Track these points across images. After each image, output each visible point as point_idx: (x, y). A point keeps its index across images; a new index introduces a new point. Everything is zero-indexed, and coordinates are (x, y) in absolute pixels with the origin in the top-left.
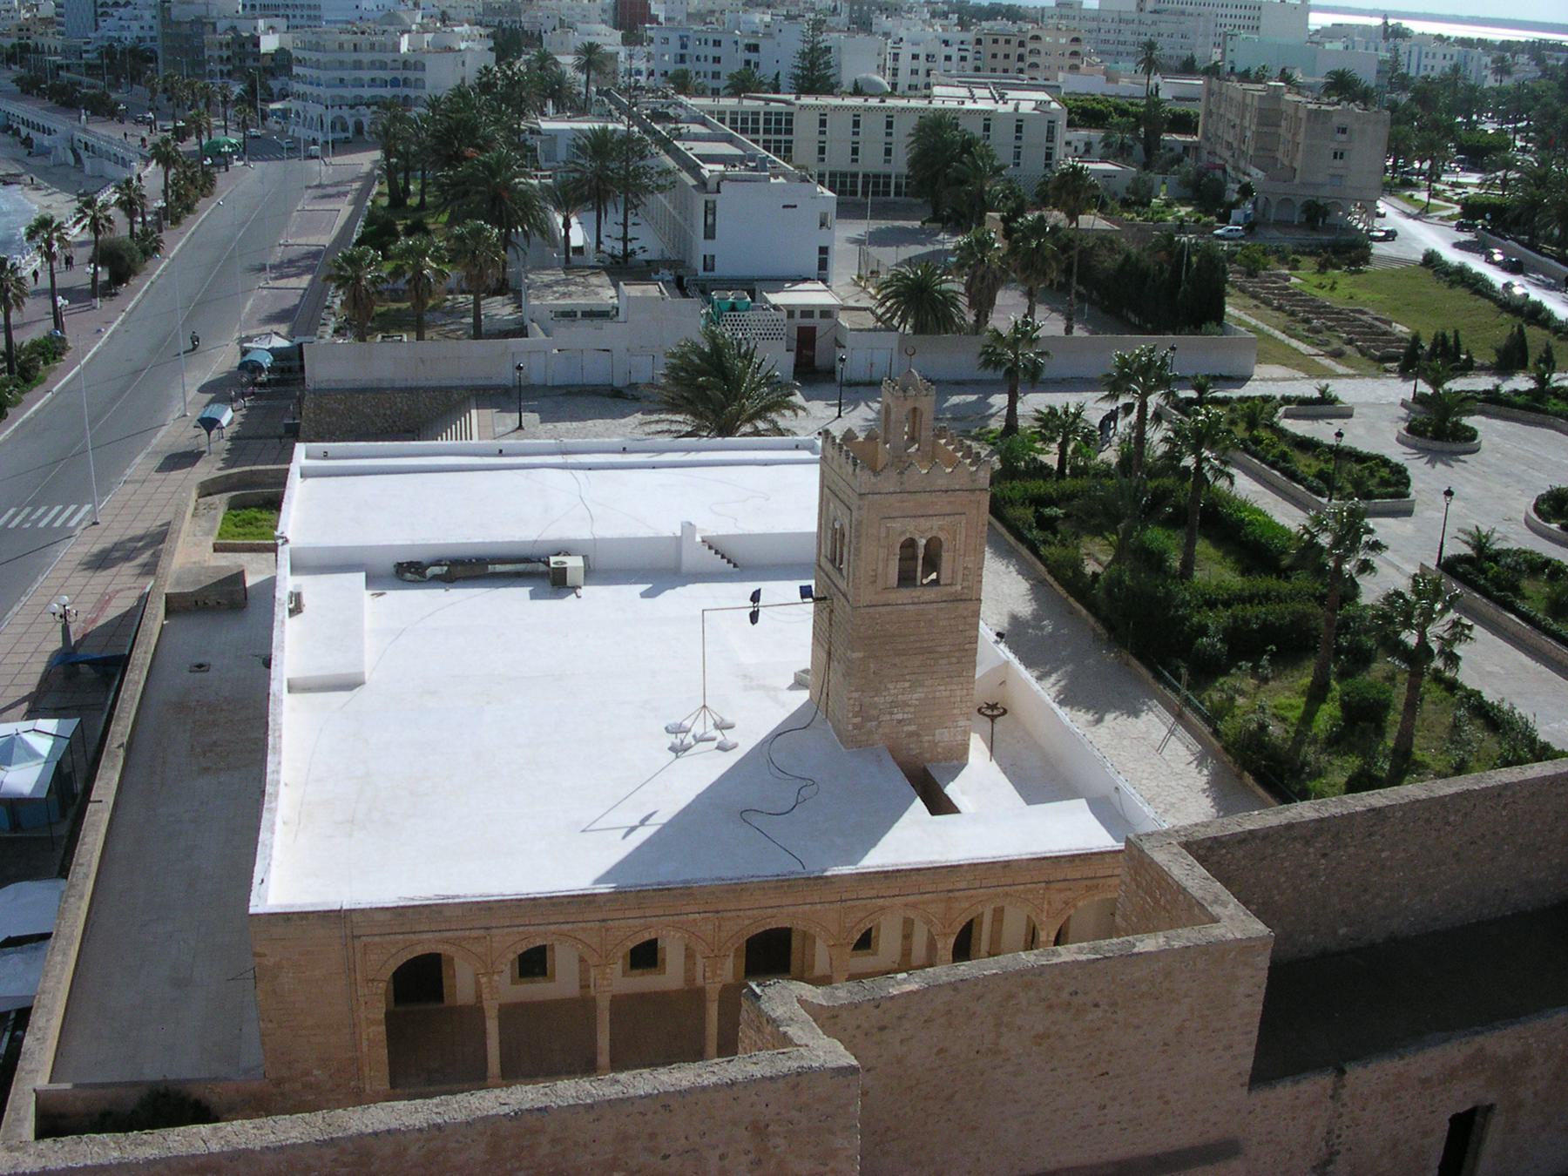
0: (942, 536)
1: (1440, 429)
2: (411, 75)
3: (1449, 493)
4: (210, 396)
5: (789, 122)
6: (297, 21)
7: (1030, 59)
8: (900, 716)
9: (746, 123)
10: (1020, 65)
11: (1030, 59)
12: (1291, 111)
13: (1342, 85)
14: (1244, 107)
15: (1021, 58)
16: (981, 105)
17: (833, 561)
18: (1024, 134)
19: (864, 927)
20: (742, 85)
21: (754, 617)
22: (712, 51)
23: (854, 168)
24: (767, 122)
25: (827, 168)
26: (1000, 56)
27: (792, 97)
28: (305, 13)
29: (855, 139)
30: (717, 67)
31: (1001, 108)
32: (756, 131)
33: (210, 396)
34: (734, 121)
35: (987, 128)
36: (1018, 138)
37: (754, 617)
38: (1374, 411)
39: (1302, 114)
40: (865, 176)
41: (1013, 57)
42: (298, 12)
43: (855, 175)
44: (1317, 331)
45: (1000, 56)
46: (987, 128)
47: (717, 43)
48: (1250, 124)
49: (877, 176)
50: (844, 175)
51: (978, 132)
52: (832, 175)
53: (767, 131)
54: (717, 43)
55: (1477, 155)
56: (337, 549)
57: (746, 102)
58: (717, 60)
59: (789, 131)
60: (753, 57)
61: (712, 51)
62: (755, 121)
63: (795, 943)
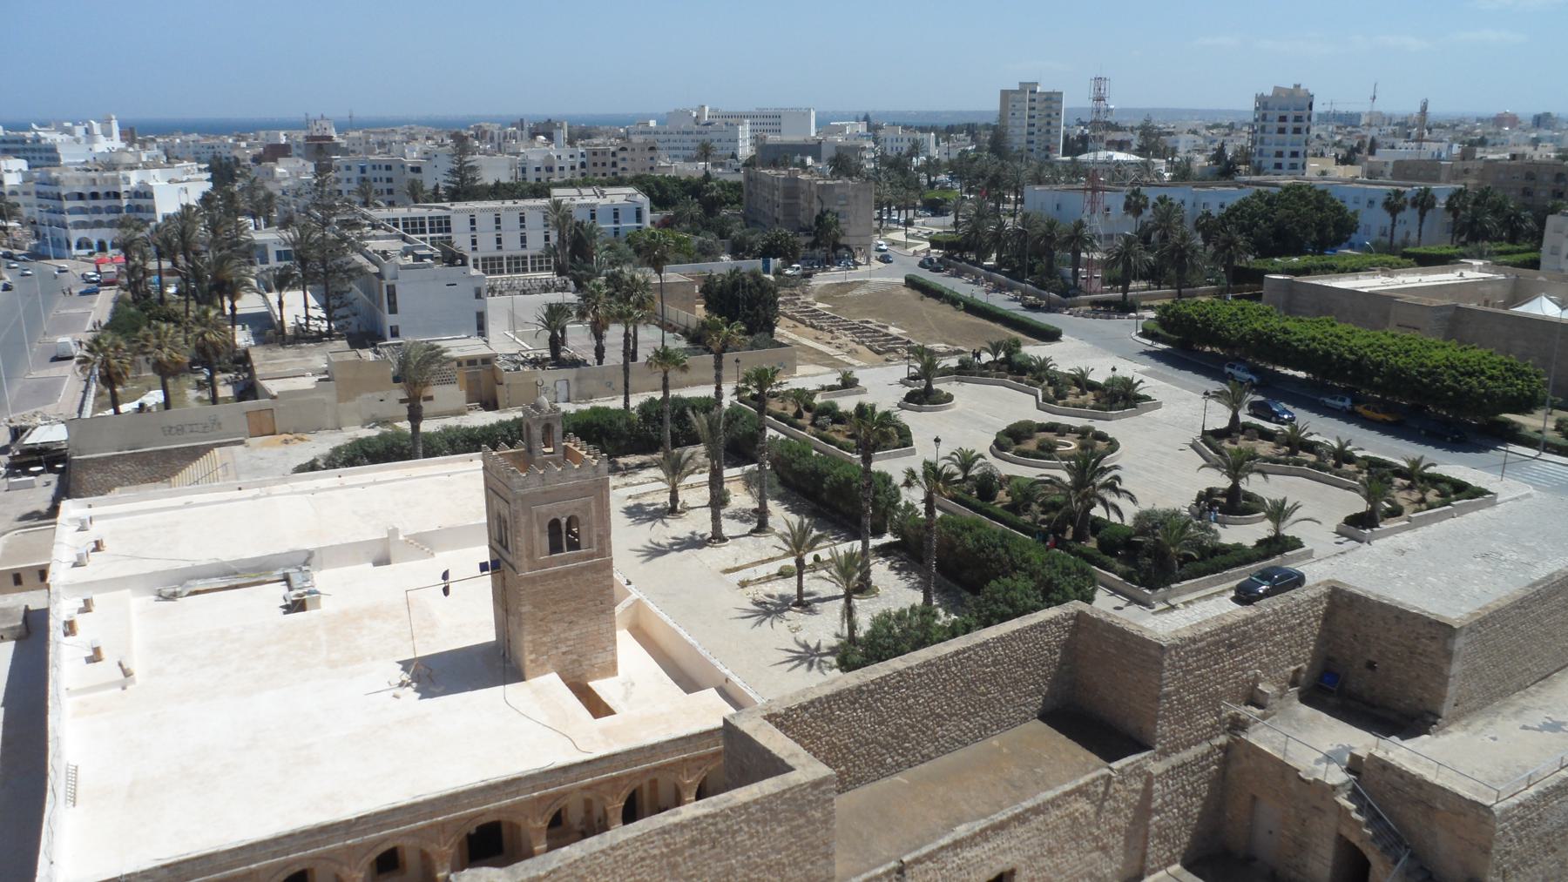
0: (578, 514)
1: (923, 397)
2: (143, 202)
3: (937, 440)
5: (448, 223)
6: (37, 162)
8: (564, 649)
9: (415, 225)
12: (805, 187)
13: (843, 163)
14: (775, 188)
15: (614, 164)
16: (587, 201)
17: (500, 542)
18: (502, 225)
19: (553, 810)
20: (416, 194)
21: (446, 591)
22: (385, 174)
24: (431, 224)
25: (479, 255)
27: (447, 205)
28: (44, 155)
30: (390, 186)
31: (602, 201)
32: (423, 231)
34: (405, 225)
35: (593, 216)
37: (446, 591)
38: (882, 387)
39: (813, 189)
42: (37, 155)
46: (593, 216)
48: (778, 197)
50: (492, 259)
51: (588, 221)
52: (484, 259)
53: (432, 231)
54: (388, 168)
55: (935, 208)
56: (960, 113)
57: (414, 210)
58: (389, 180)
59: (448, 230)
60: (417, 176)
61: (385, 174)
62: (422, 224)
63: (505, 831)
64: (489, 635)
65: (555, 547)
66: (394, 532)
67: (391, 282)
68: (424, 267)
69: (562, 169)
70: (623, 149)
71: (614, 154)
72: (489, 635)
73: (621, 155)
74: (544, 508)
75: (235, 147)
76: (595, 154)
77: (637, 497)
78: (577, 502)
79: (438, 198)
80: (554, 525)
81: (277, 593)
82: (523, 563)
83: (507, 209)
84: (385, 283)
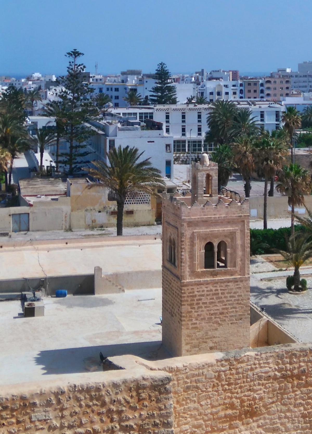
4: (45, 371)
7: (266, 92)
10: (262, 95)
11: (266, 92)
15: (262, 91)
18: (186, 120)
22: (114, 94)
23: (183, 138)
26: (252, 91)
27: (152, 106)
29: (199, 124)
33: (45, 371)
36: (184, 122)
40: (189, 142)
41: (258, 91)
43: (184, 141)
44: (165, 275)
45: (252, 91)
47: (117, 90)
49: (194, 142)
54: (117, 90)
64: (158, 337)
65: (209, 263)
66: (98, 269)
67: (112, 138)
68: (134, 130)
69: (227, 93)
70: (269, 82)
71: (262, 85)
72: (158, 337)
73: (267, 85)
74: (203, 230)
75: (25, 83)
76: (249, 84)
77: (270, 280)
78: (230, 228)
79: (145, 103)
80: (209, 247)
81: (16, 307)
82: (187, 271)
83: (190, 109)
84: (108, 139)
